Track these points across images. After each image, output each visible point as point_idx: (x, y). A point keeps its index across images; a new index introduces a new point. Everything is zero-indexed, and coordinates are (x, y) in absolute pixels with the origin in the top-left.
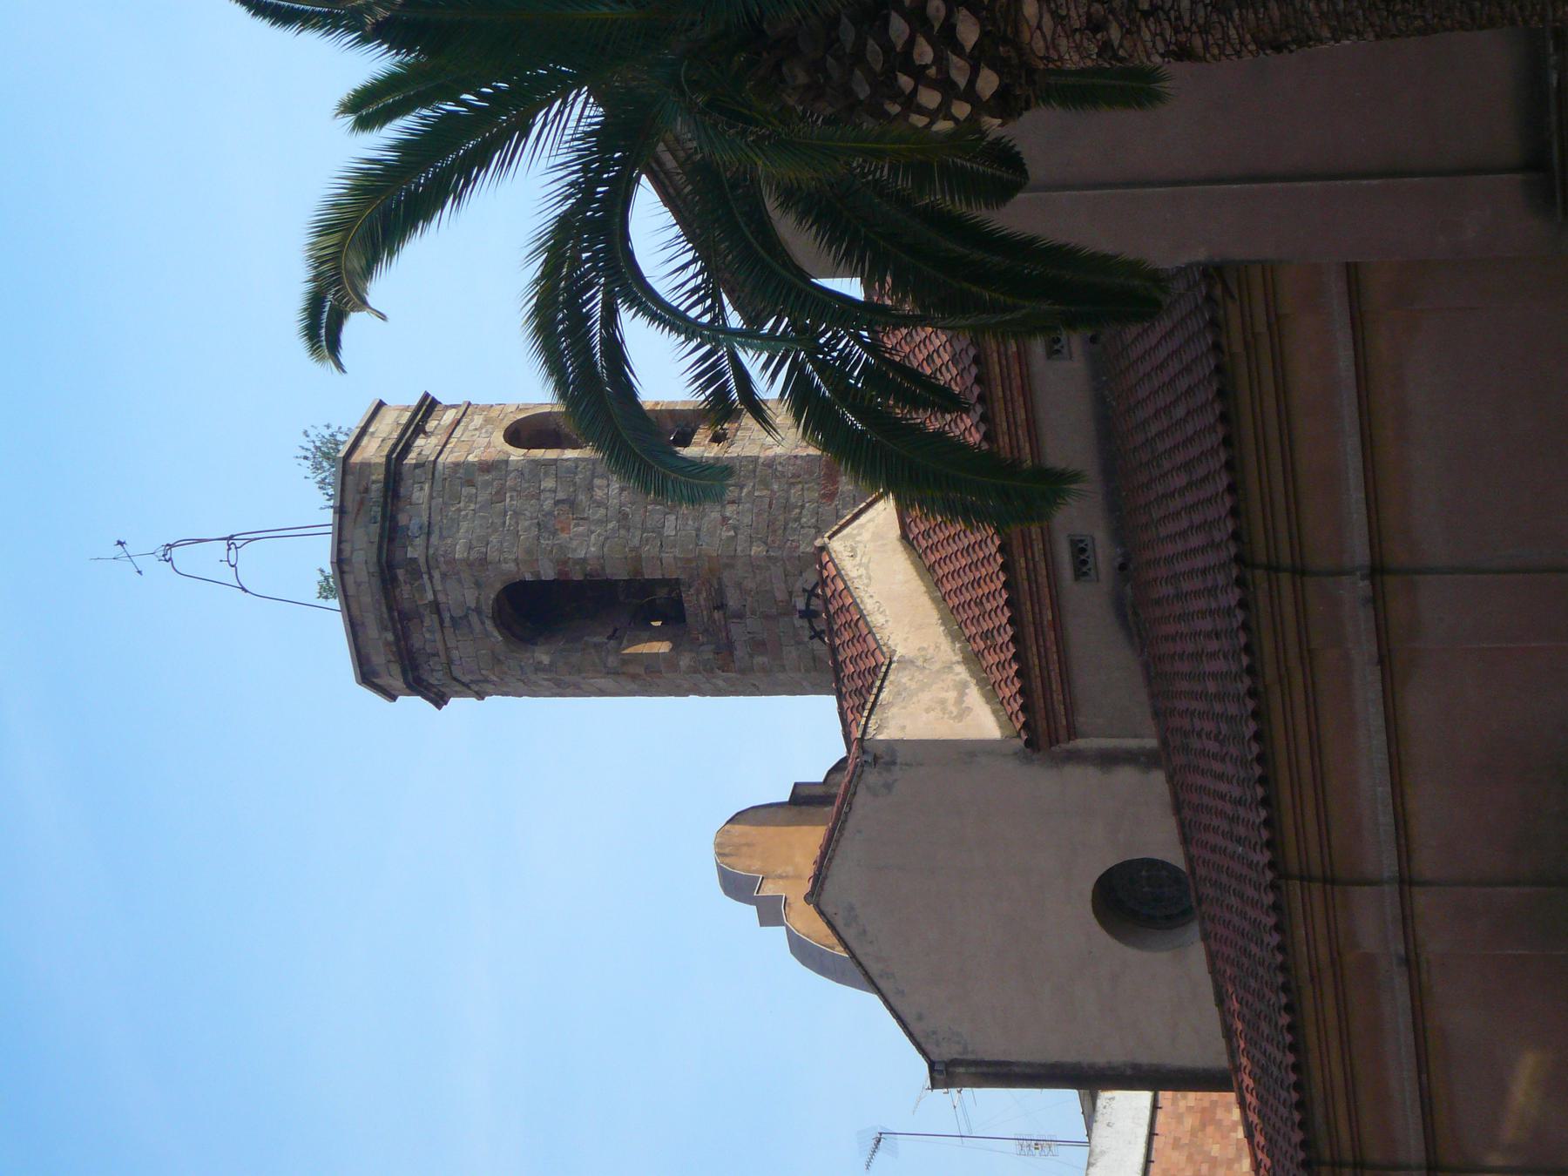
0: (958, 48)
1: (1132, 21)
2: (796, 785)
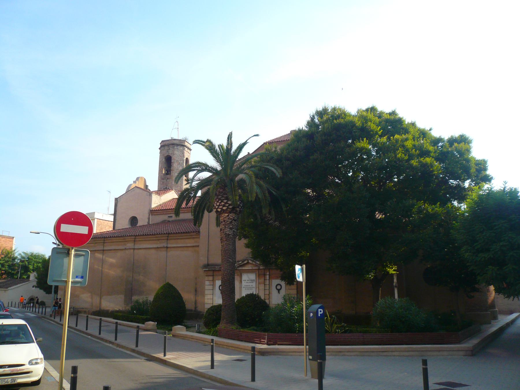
0: (223, 207)
2: (148, 186)
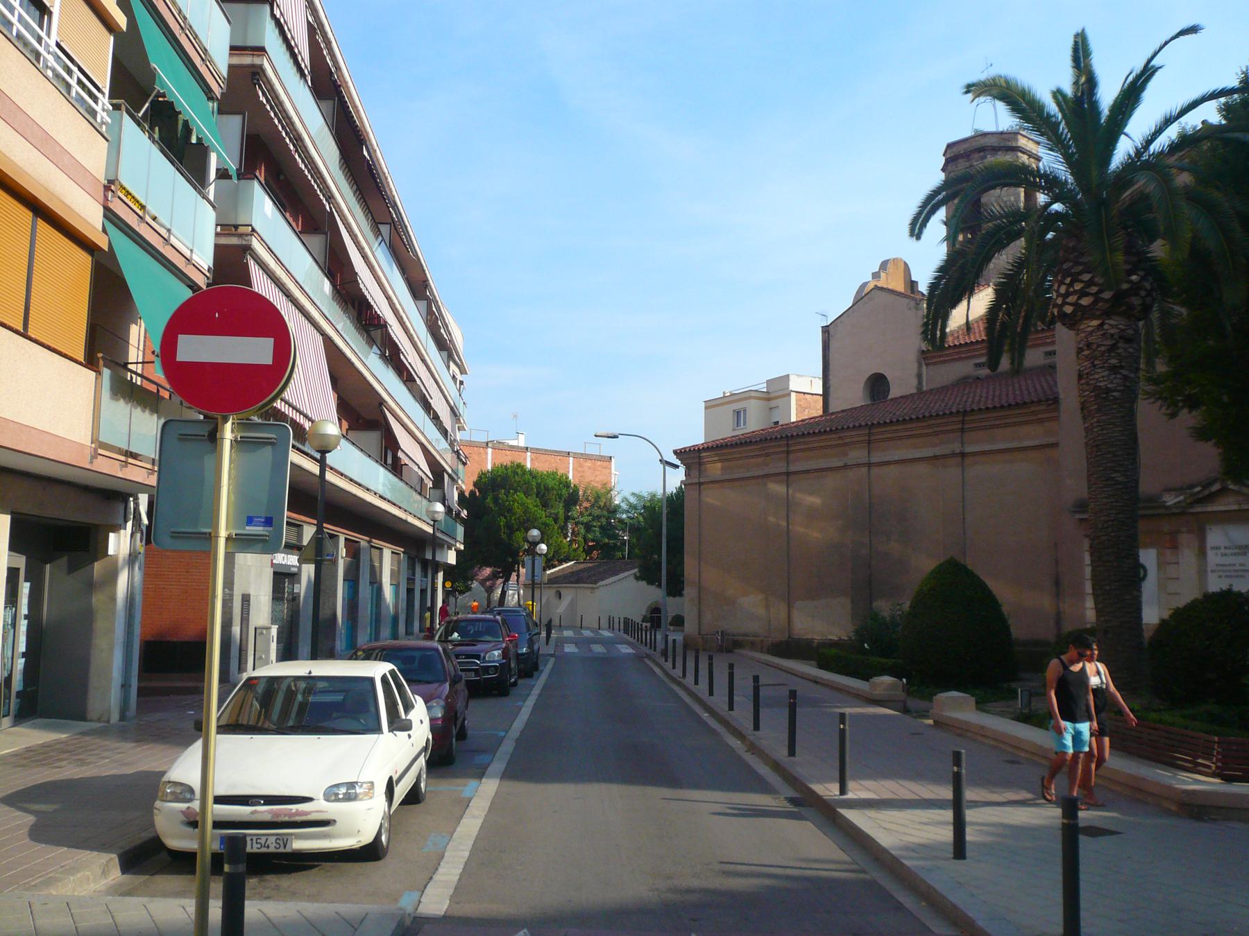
0: (1079, 298)
1: (1091, 358)
2: (917, 282)
